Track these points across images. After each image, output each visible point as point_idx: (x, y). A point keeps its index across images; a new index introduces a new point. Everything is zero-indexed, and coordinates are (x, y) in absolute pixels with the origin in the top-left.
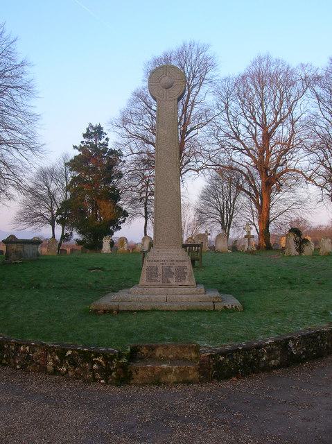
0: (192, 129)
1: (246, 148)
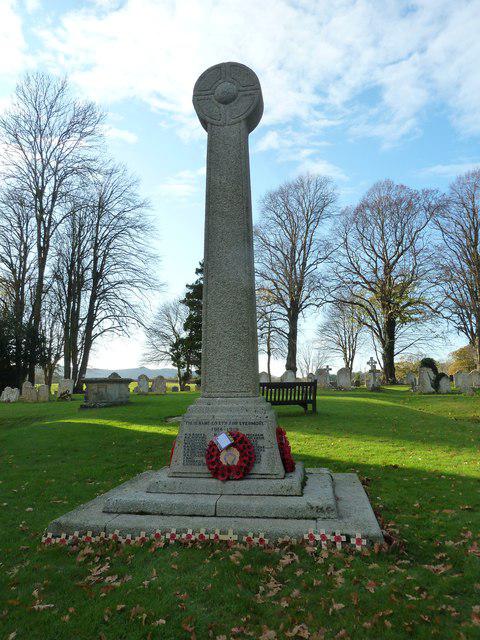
0: (311, 265)
1: (367, 282)
